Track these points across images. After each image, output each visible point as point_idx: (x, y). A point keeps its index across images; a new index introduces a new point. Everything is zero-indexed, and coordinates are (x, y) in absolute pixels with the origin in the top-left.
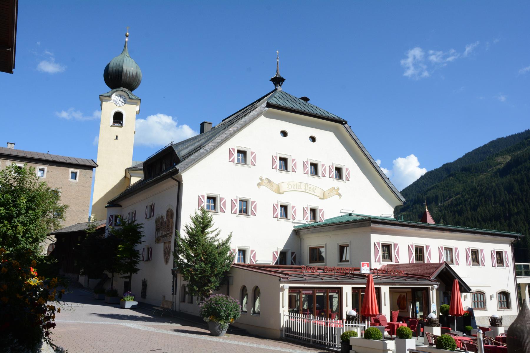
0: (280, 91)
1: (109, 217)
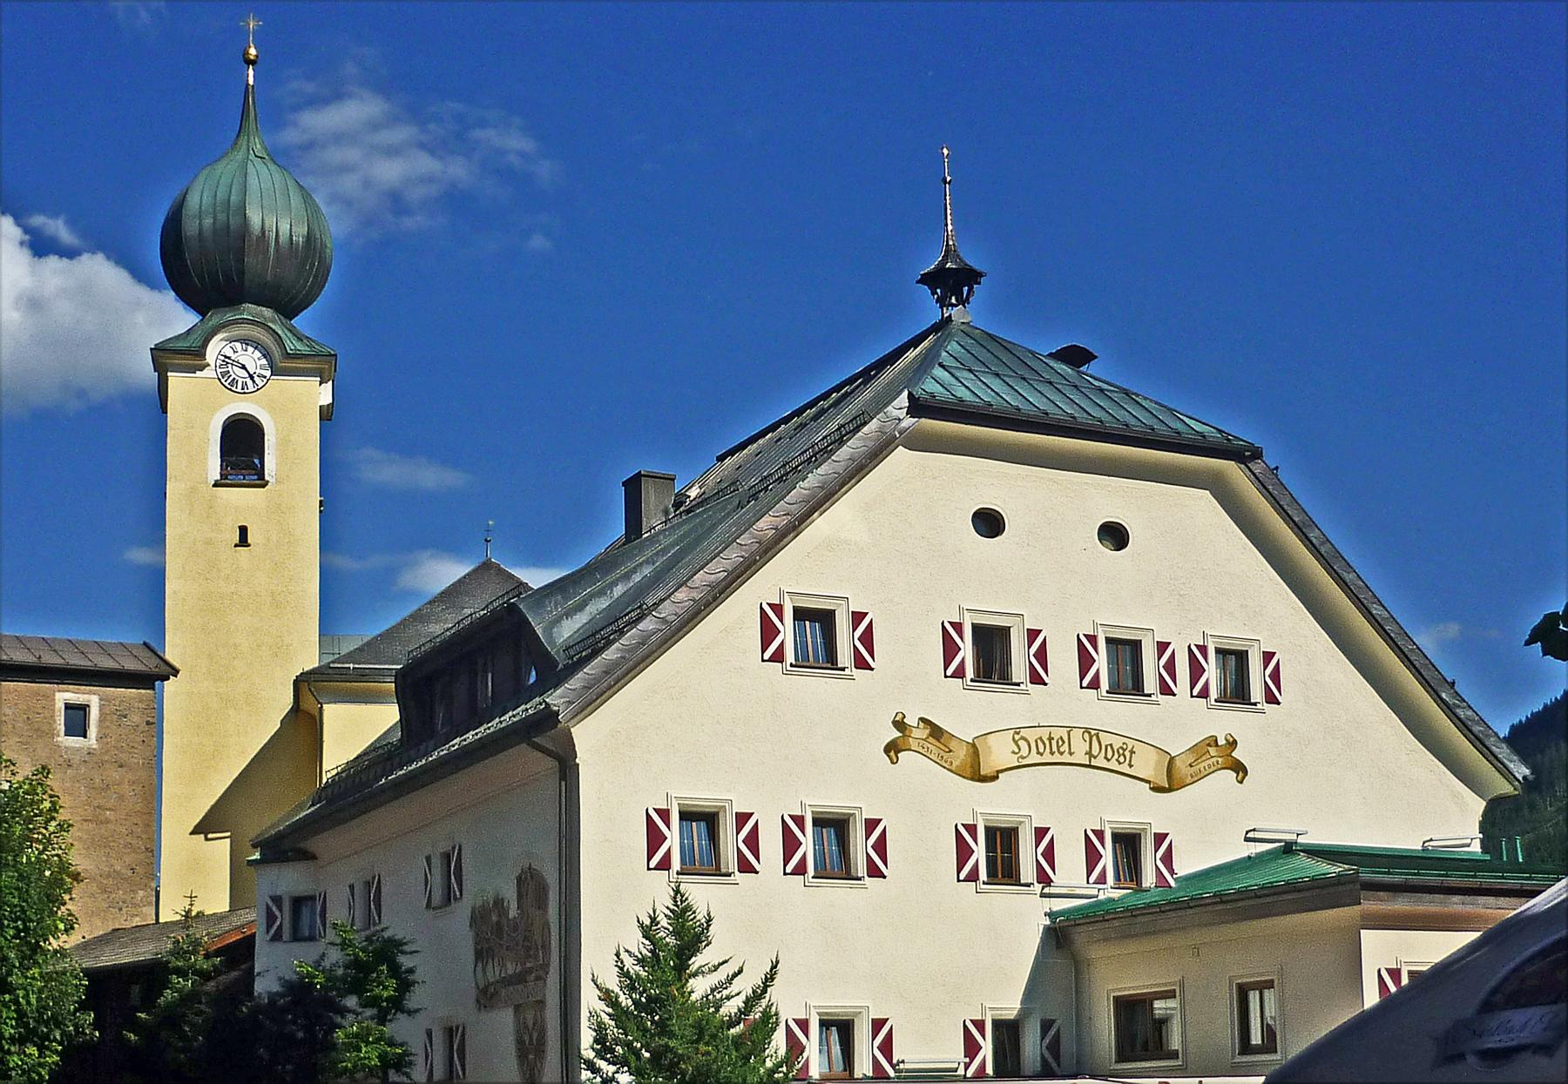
0: (962, 327)
1: (267, 905)
